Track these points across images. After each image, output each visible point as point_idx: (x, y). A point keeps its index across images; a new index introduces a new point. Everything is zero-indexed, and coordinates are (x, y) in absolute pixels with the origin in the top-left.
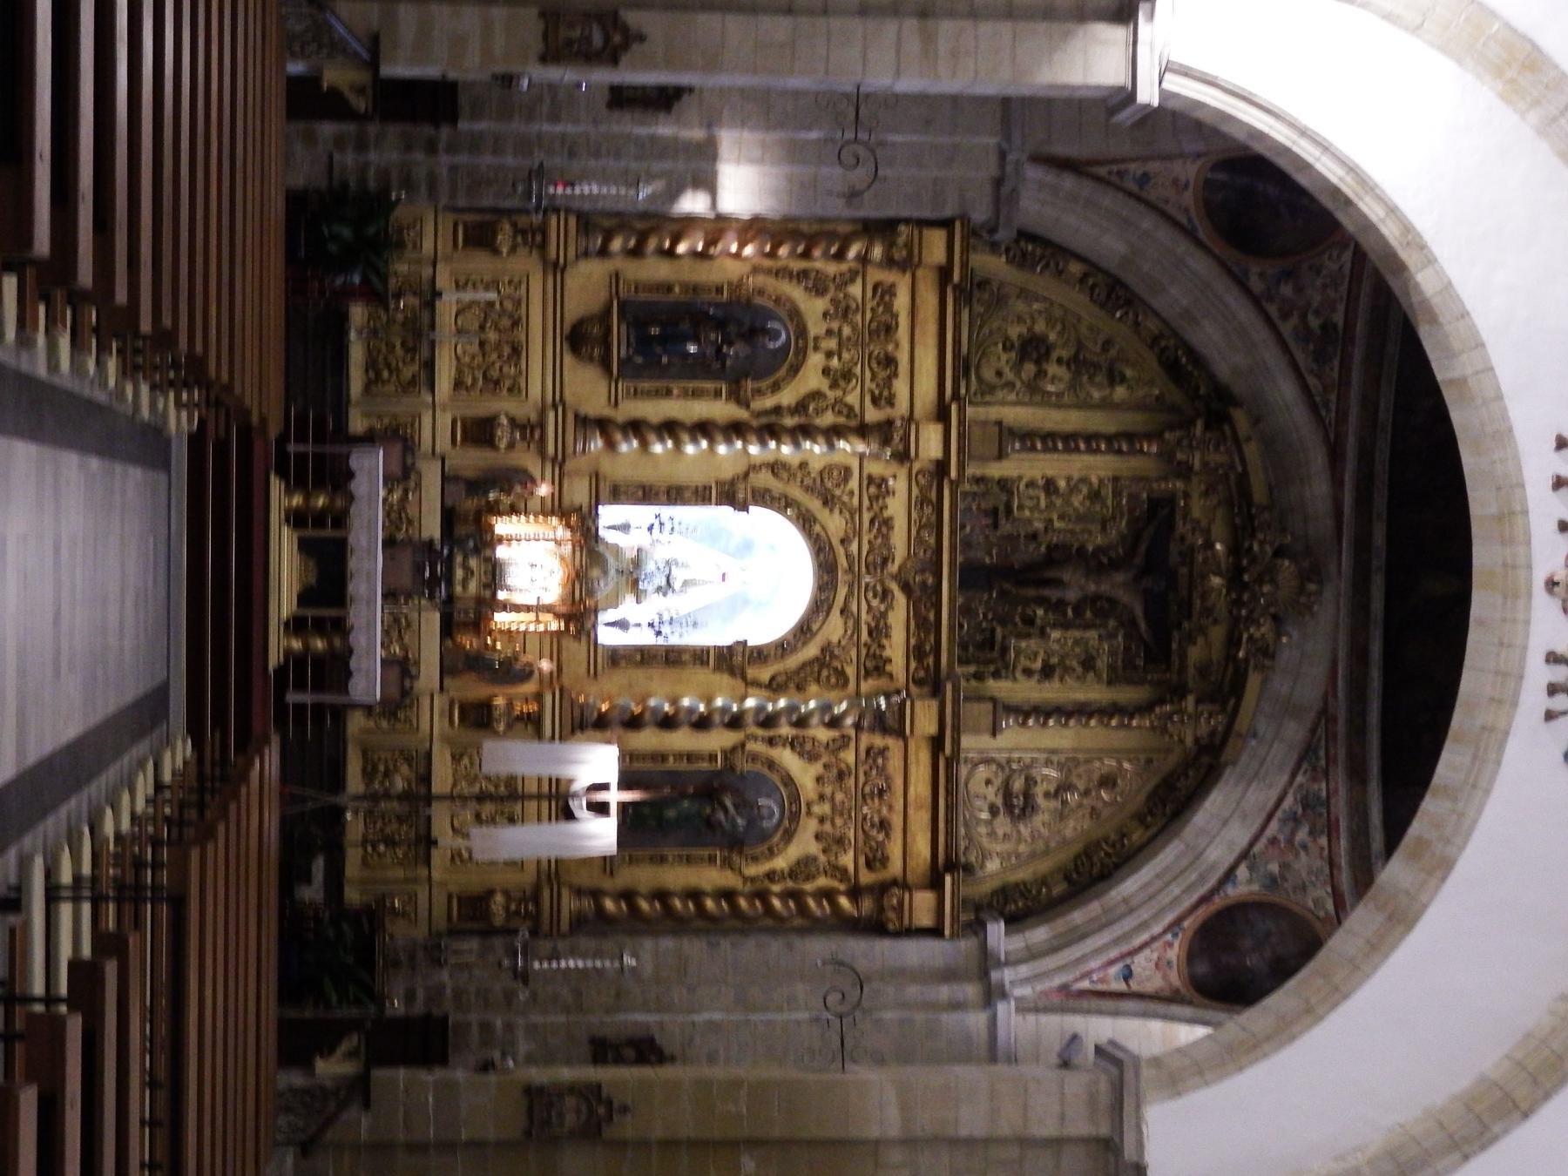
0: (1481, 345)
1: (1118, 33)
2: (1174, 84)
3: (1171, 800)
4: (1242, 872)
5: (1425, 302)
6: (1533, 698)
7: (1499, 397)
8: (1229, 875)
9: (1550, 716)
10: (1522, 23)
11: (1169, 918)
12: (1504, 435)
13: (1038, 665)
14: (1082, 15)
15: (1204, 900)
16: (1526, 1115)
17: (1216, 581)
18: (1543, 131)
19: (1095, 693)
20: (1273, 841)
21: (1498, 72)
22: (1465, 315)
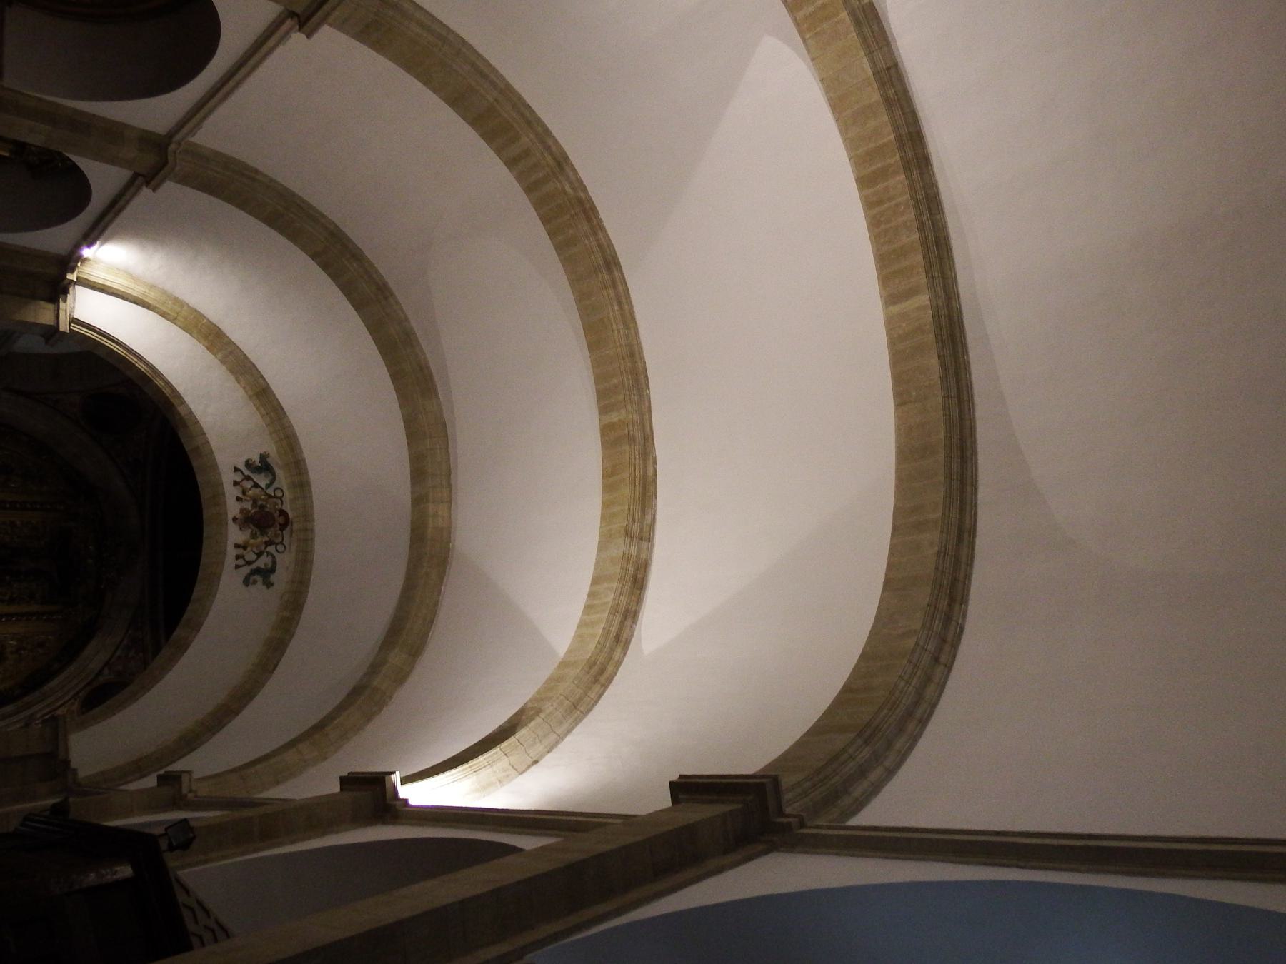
0: (204, 434)
1: (51, 306)
2: (75, 327)
3: (70, 651)
4: (106, 671)
5: (181, 418)
6: (230, 560)
7: (212, 452)
8: (100, 672)
9: (237, 567)
10: (214, 319)
11: (72, 693)
12: (214, 466)
13: (7, 598)
14: (34, 297)
15: (89, 684)
16: (237, 714)
17: (90, 561)
18: (223, 362)
19: (34, 608)
20: (119, 657)
21: (206, 337)
22: (198, 422)
